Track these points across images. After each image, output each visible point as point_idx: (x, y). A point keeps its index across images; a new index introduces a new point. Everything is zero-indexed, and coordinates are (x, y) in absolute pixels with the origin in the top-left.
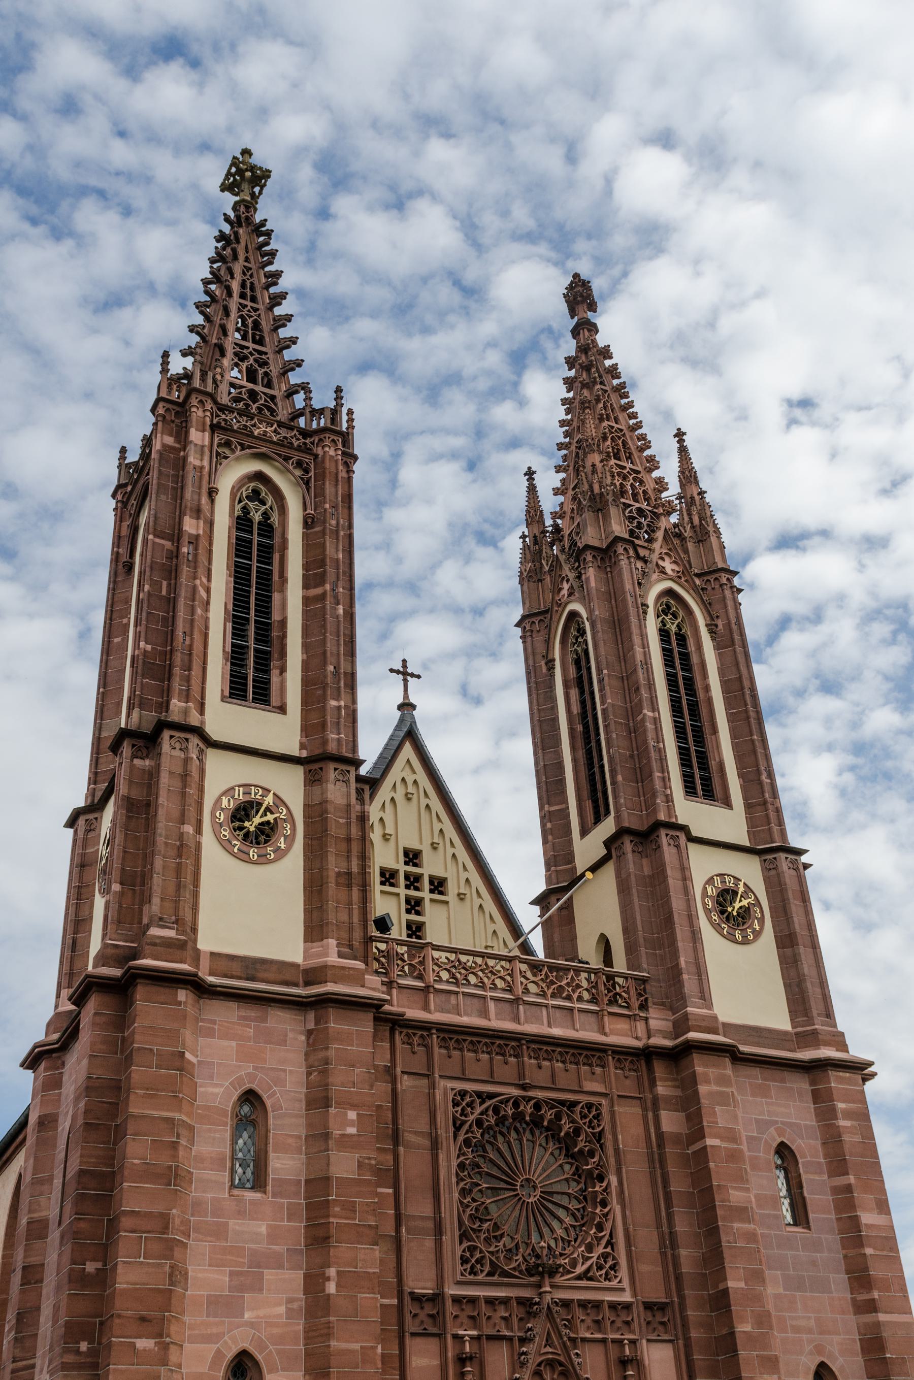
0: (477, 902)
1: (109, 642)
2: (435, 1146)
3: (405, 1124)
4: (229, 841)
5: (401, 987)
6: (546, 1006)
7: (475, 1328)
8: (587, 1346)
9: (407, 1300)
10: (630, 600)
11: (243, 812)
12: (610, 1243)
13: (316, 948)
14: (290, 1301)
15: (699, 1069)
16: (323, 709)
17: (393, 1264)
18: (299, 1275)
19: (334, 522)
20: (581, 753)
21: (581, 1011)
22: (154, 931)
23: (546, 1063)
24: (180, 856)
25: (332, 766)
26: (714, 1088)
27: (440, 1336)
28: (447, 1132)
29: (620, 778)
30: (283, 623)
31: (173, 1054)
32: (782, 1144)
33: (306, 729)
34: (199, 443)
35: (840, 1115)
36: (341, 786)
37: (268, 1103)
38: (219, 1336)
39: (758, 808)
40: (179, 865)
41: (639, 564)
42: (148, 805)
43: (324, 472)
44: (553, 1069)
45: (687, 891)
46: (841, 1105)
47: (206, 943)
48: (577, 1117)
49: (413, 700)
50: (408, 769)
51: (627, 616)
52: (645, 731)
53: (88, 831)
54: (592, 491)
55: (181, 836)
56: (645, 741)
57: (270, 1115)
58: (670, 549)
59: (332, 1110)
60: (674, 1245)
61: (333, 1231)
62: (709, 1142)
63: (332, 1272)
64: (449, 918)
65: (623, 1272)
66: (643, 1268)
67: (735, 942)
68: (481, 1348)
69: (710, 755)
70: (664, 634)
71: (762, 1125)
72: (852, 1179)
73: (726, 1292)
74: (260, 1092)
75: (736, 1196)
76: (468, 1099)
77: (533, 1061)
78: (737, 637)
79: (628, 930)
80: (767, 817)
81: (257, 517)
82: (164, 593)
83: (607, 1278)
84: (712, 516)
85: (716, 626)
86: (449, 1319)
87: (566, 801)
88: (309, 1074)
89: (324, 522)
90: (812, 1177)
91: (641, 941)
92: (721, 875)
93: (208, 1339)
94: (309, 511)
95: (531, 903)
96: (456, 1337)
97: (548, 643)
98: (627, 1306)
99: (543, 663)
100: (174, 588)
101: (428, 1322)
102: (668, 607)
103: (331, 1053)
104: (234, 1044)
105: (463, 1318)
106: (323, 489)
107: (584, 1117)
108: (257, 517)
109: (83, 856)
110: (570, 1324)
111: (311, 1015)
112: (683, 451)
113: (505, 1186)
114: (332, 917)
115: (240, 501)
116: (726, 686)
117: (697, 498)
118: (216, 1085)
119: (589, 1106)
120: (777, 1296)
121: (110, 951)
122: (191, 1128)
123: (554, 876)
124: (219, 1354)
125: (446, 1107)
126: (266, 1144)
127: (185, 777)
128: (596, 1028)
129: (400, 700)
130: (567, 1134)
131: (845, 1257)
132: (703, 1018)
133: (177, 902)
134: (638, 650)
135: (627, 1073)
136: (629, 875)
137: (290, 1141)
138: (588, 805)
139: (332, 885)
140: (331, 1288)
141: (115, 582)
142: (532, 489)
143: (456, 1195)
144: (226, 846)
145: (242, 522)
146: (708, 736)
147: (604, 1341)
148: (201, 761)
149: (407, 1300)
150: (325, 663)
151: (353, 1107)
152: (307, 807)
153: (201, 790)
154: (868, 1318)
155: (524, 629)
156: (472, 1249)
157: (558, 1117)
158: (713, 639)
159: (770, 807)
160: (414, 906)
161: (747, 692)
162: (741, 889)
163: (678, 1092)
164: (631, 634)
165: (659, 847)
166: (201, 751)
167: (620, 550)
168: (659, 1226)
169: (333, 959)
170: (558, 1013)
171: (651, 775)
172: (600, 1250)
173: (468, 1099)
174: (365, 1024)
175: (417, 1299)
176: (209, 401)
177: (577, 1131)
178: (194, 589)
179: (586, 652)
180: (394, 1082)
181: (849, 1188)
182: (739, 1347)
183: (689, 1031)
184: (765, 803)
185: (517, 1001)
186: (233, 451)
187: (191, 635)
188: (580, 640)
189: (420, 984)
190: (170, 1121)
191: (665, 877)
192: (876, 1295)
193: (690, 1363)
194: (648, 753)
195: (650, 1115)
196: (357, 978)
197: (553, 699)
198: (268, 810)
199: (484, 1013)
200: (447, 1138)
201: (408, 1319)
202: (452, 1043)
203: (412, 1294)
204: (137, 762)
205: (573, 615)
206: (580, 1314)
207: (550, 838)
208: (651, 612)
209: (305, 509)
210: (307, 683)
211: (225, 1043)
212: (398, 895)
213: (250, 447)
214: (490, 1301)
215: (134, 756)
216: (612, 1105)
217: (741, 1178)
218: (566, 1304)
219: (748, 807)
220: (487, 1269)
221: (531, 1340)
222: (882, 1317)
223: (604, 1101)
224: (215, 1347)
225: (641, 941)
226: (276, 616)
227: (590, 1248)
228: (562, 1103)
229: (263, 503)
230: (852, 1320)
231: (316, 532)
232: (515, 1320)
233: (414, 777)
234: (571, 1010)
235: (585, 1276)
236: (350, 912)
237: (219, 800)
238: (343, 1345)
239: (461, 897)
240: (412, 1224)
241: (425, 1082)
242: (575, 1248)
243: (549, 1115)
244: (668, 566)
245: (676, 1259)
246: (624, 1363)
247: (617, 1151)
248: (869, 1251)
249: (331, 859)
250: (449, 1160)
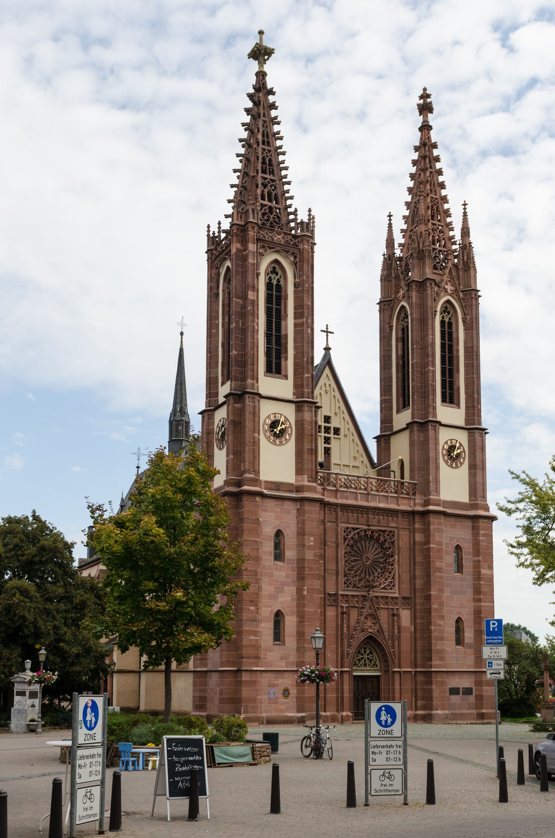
0: (352, 438)
1: (210, 331)
2: (337, 546)
3: (328, 539)
4: (269, 437)
5: (328, 490)
6: (379, 495)
7: (347, 604)
8: (382, 610)
9: (327, 595)
10: (429, 310)
11: (274, 424)
12: (393, 578)
13: (300, 478)
14: (292, 596)
15: (431, 520)
16: (302, 378)
17: (323, 585)
18: (295, 588)
19: (307, 285)
20: (400, 374)
21: (391, 497)
22: (247, 475)
23: (377, 517)
24: (254, 446)
25: (306, 405)
26: (436, 527)
27: (337, 606)
28: (341, 541)
29: (415, 397)
30: (286, 336)
31: (256, 519)
32: (458, 545)
33: (296, 386)
34: (252, 250)
35: (481, 535)
36: (309, 413)
37: (285, 534)
38: (272, 606)
39: (471, 408)
40: (254, 449)
41: (436, 289)
42: (240, 423)
43: (303, 258)
44: (379, 518)
45: (436, 449)
46: (482, 532)
47: (263, 477)
48: (386, 536)
49: (330, 346)
50: (327, 379)
51: (427, 318)
52: (428, 376)
53: (209, 419)
54: (419, 248)
55: (254, 438)
56: (428, 381)
57: (286, 538)
58: (451, 278)
59: (306, 537)
60: (415, 578)
61: (306, 576)
62: (432, 546)
63: (305, 588)
64: (340, 445)
65: (396, 587)
66: (403, 586)
67: (453, 468)
68: (349, 610)
69: (455, 383)
70: (442, 323)
71: (451, 539)
72: (481, 558)
73: (430, 595)
74: (282, 530)
75: (438, 564)
76: (349, 530)
77: (372, 516)
78: (474, 325)
79: (411, 462)
80: (474, 412)
81: (275, 282)
82: (240, 326)
83: (391, 589)
84: (473, 257)
85: (466, 319)
86: (339, 601)
87: (391, 395)
88: (298, 524)
89: (303, 286)
90: (466, 556)
91: (416, 468)
92: (451, 440)
93: (268, 606)
94: (297, 280)
95: (374, 438)
96: (341, 606)
97: (391, 317)
98: (397, 598)
99: (388, 326)
100: (244, 324)
101: (333, 602)
102: (446, 308)
103: (306, 517)
104: (273, 514)
105: (344, 601)
106: (303, 268)
107: (388, 535)
108: (275, 282)
109: (208, 429)
110: (378, 603)
111: (299, 503)
112: (465, 214)
113: (359, 558)
114: (305, 467)
115: (268, 275)
116: (466, 348)
117: (468, 245)
118: (269, 528)
119: (390, 532)
120: (447, 596)
121: (231, 481)
122: (262, 543)
123: (383, 428)
124: (272, 611)
125: (342, 534)
126: (284, 547)
127: (254, 413)
128: (395, 503)
129: (324, 346)
130: (382, 541)
131: (474, 584)
132: (436, 500)
133: (254, 464)
134: (430, 337)
135: (405, 519)
136: (414, 440)
137: (292, 546)
138: (401, 399)
139: (306, 454)
140: (305, 593)
141: (211, 301)
142: (390, 226)
143: (344, 562)
144: (268, 439)
145: (269, 286)
146: (455, 374)
147: (388, 608)
148: (259, 405)
149: (327, 595)
150: (303, 357)
151: (313, 536)
152: (297, 421)
153: (259, 420)
154: (478, 604)
155: (380, 307)
156: (348, 580)
157: (379, 535)
158: (464, 325)
159: (476, 408)
160: (327, 440)
161: (475, 353)
162: (458, 445)
163: (423, 527)
164: (428, 329)
165: (428, 430)
166: (259, 401)
167: (428, 284)
168: (410, 572)
169: (306, 483)
170: (382, 498)
171: (428, 397)
172: (390, 580)
173: (349, 530)
174: (316, 507)
175: (330, 595)
176: (256, 226)
177: (385, 541)
178: (254, 326)
179: (408, 326)
180: (325, 525)
181: (479, 561)
182: (432, 611)
183: (429, 505)
184: (474, 407)
185: (368, 494)
186: (266, 251)
187: (253, 349)
188: (405, 320)
189: (335, 489)
190: (256, 541)
191: (428, 444)
192: (482, 597)
193: (415, 616)
194: (429, 387)
195: (412, 534)
196: (314, 490)
197: (391, 346)
198: (283, 423)
199: (356, 499)
200: (342, 544)
201: (327, 601)
202: (345, 510)
203: (328, 593)
204: (236, 405)
205: (403, 307)
206: (381, 600)
207: (384, 411)
208: (438, 314)
209: (295, 278)
210: (296, 365)
211: (270, 514)
212: (321, 436)
213: (273, 248)
214: (352, 596)
215: (235, 403)
216: (399, 531)
217: (441, 558)
218: (377, 597)
219: (467, 407)
220: (352, 586)
221: (365, 608)
222: (482, 604)
223: (396, 530)
224: (270, 609)
225: (416, 468)
226: (283, 332)
227: (386, 580)
228: (381, 531)
229: (277, 274)
230: (472, 604)
231: (299, 290)
232: (360, 602)
233: (329, 382)
234: (387, 496)
235: (384, 588)
236: (312, 464)
237: (265, 421)
238: (309, 609)
239: (345, 436)
240: (329, 571)
241: (335, 524)
242: (381, 580)
243: (376, 535)
244: (449, 288)
245: (415, 583)
246: (394, 615)
247: (399, 547)
248: (482, 582)
249: (306, 444)
250: (342, 551)
